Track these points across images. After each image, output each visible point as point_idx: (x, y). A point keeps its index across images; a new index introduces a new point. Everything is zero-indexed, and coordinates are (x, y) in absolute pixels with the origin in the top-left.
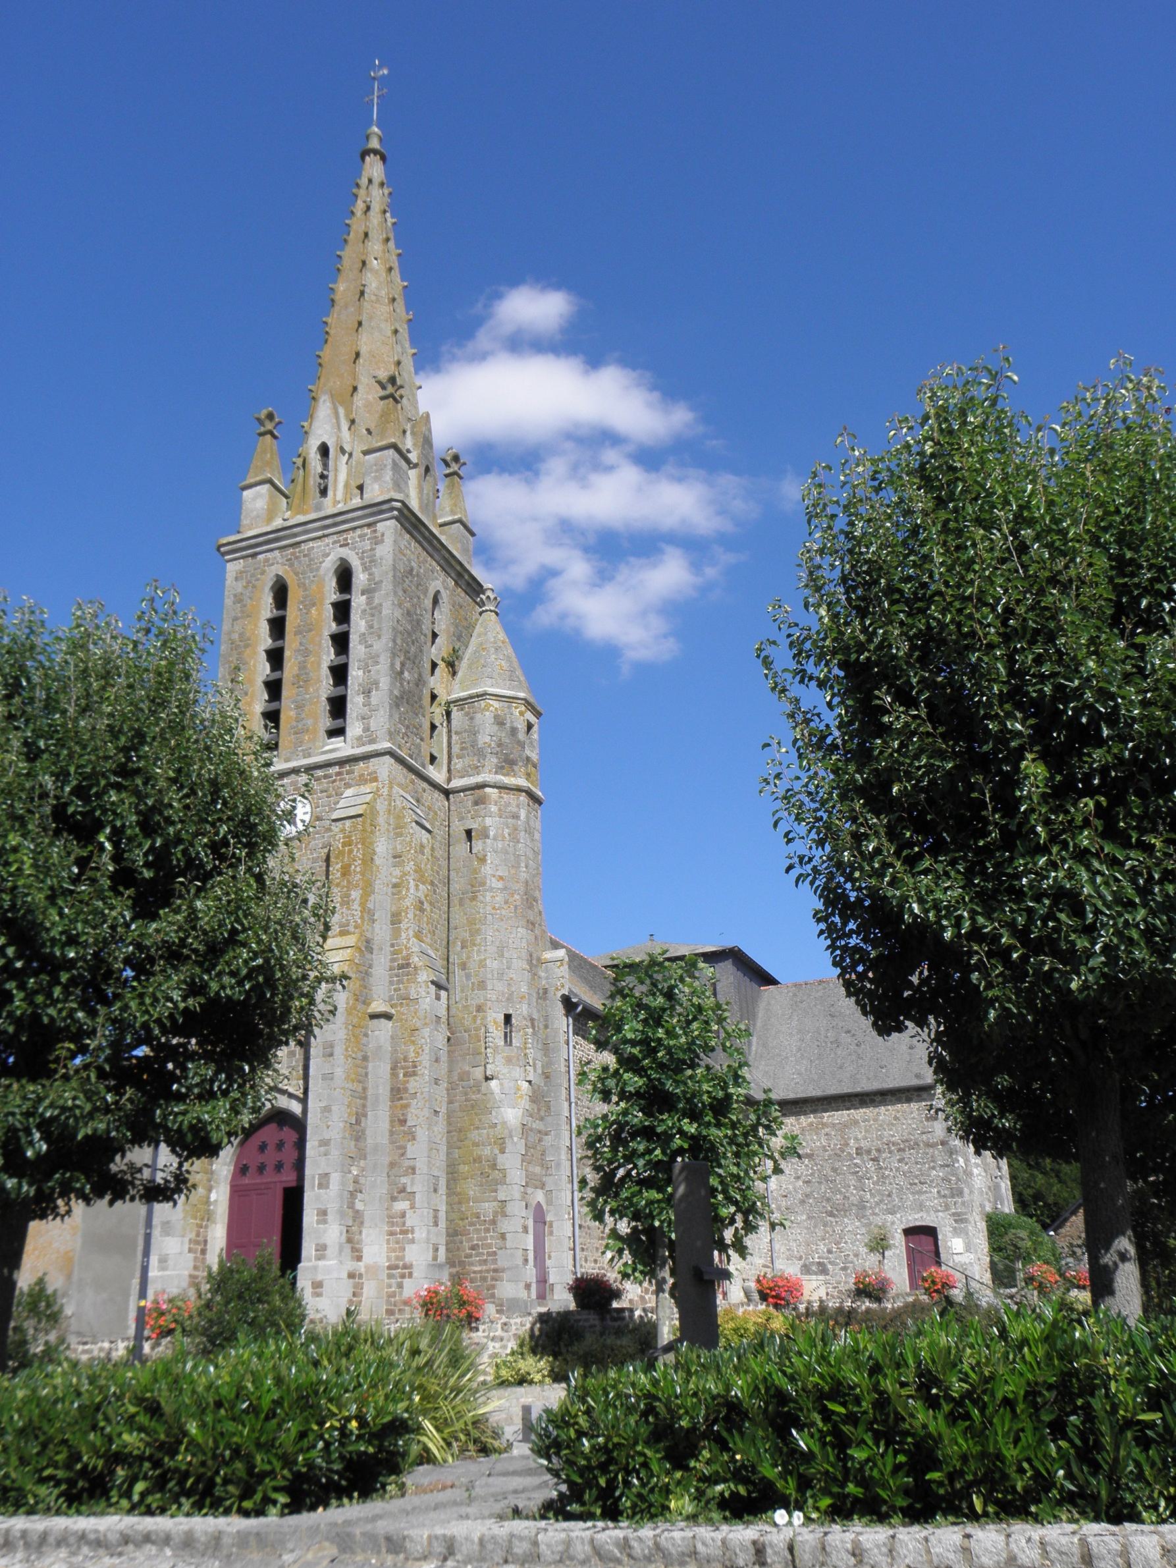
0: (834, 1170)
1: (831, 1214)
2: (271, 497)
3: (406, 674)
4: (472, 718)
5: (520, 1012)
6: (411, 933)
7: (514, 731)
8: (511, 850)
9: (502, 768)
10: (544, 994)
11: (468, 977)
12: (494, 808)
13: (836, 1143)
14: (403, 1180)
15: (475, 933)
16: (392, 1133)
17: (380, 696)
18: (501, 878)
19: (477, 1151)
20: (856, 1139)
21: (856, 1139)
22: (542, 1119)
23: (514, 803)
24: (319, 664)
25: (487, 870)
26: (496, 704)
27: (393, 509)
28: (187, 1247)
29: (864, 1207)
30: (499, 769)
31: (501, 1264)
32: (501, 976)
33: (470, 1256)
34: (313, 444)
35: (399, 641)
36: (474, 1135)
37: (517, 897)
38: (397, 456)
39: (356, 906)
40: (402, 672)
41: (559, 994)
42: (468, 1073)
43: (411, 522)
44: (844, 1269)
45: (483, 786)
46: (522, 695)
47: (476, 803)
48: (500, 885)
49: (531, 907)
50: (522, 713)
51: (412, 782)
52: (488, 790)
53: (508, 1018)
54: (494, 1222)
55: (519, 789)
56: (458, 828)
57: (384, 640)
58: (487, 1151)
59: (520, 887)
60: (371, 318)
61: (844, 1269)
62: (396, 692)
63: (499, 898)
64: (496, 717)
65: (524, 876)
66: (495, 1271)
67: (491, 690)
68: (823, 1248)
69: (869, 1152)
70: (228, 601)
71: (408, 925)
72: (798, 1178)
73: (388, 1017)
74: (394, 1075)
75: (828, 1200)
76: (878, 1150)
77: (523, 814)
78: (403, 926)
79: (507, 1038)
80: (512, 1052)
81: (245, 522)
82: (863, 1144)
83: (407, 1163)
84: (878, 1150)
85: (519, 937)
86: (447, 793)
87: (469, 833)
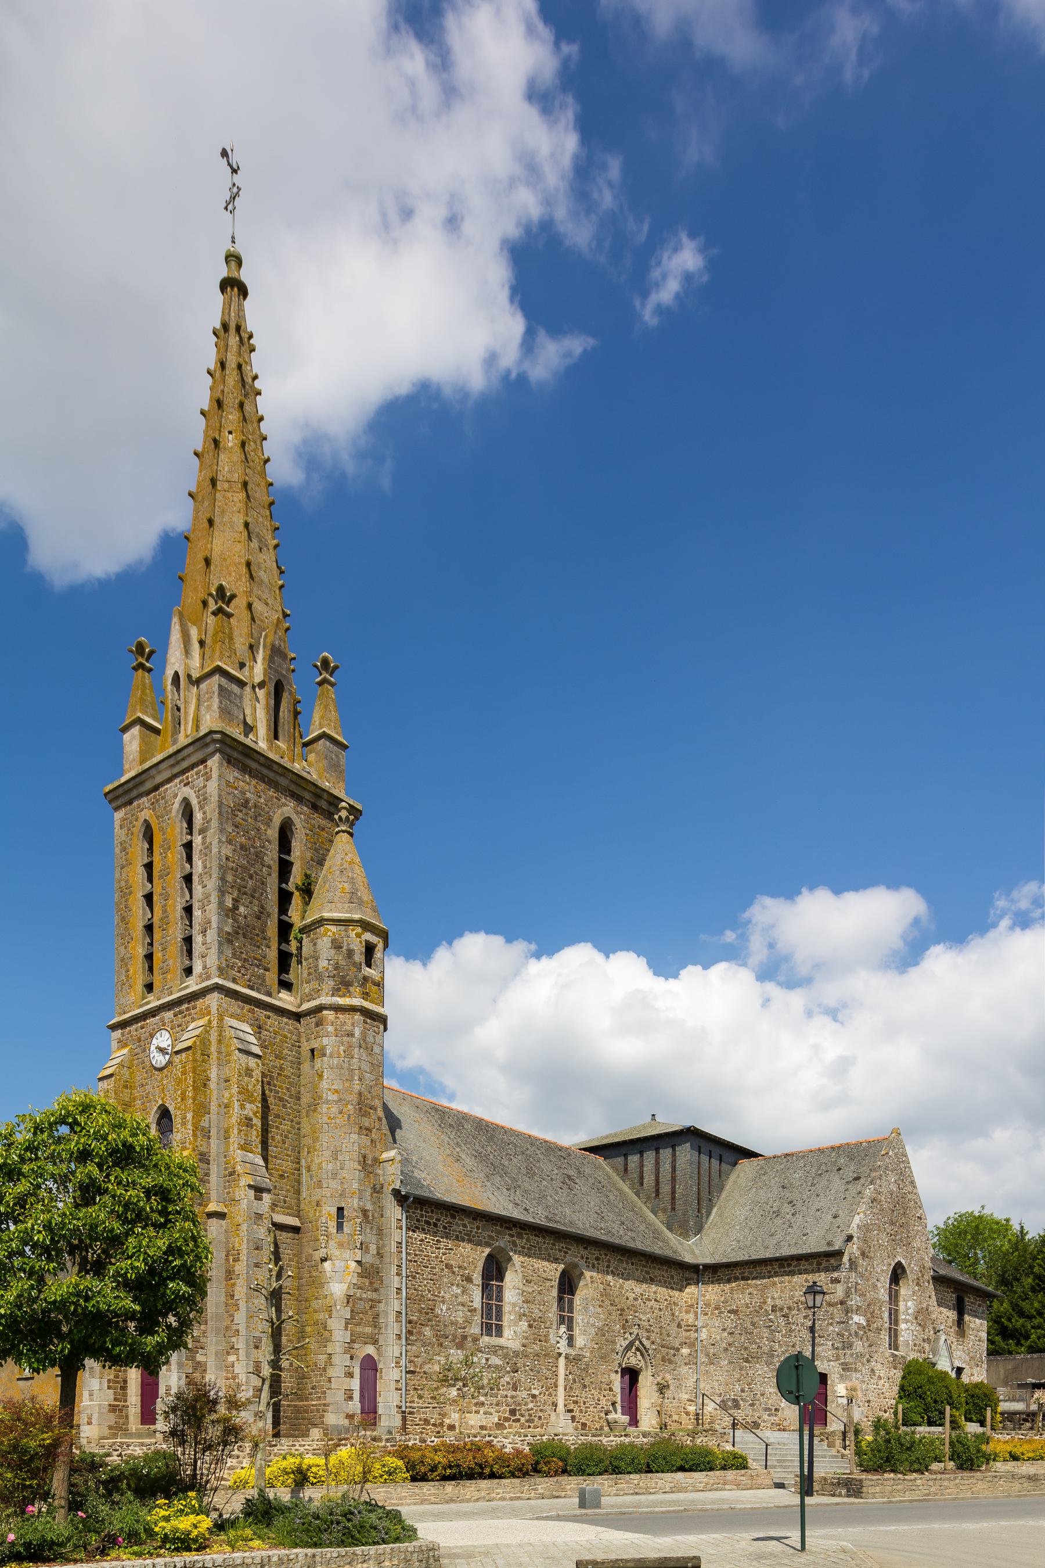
0: (753, 1324)
1: (747, 1361)
2: (143, 738)
3: (242, 909)
4: (315, 944)
5: (352, 1205)
6: (236, 1146)
7: (350, 953)
8: (346, 1065)
9: (339, 990)
10: (377, 1190)
11: (311, 1177)
12: (330, 1029)
13: (756, 1300)
14: (234, 1339)
15: (315, 1140)
16: (227, 1305)
17: (212, 935)
18: (336, 1091)
19: (316, 1316)
20: (773, 1298)
21: (773, 1298)
22: (376, 1290)
23: (349, 1022)
24: (175, 907)
25: (324, 1085)
26: (333, 928)
27: (215, 741)
28: (106, 1385)
29: (773, 1355)
30: (335, 992)
31: (328, 1400)
32: (334, 1176)
33: (311, 1394)
34: (169, 674)
35: (230, 878)
36: (315, 1304)
37: (350, 1107)
38: (224, 682)
39: (190, 1126)
40: (235, 908)
41: (391, 1188)
42: (311, 1255)
43: (239, 755)
44: (752, 1405)
45: (320, 1009)
46: (356, 917)
47: (317, 1025)
48: (335, 1097)
49: (366, 1114)
50: (358, 935)
51: (252, 1012)
52: (325, 1012)
53: (340, 1210)
54: (325, 1370)
55: (353, 1009)
56: (306, 1047)
57: (213, 880)
58: (321, 1316)
59: (353, 1098)
60: (223, 512)
61: (752, 1405)
62: (228, 929)
63: (334, 1109)
64: (333, 941)
65: (357, 1086)
66: (325, 1405)
67: (327, 915)
68: (738, 1388)
69: (781, 1309)
70: (117, 850)
71: (235, 1139)
72: (724, 1330)
73: (221, 1216)
74: (227, 1260)
75: (746, 1349)
76: (789, 1308)
77: (357, 1032)
78: (231, 1140)
79: (340, 1227)
80: (342, 1237)
81: (126, 767)
82: (778, 1302)
83: (235, 1327)
84: (789, 1308)
85: (352, 1143)
86: (297, 1017)
87: (312, 1051)
